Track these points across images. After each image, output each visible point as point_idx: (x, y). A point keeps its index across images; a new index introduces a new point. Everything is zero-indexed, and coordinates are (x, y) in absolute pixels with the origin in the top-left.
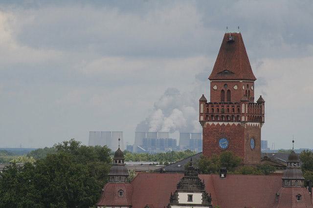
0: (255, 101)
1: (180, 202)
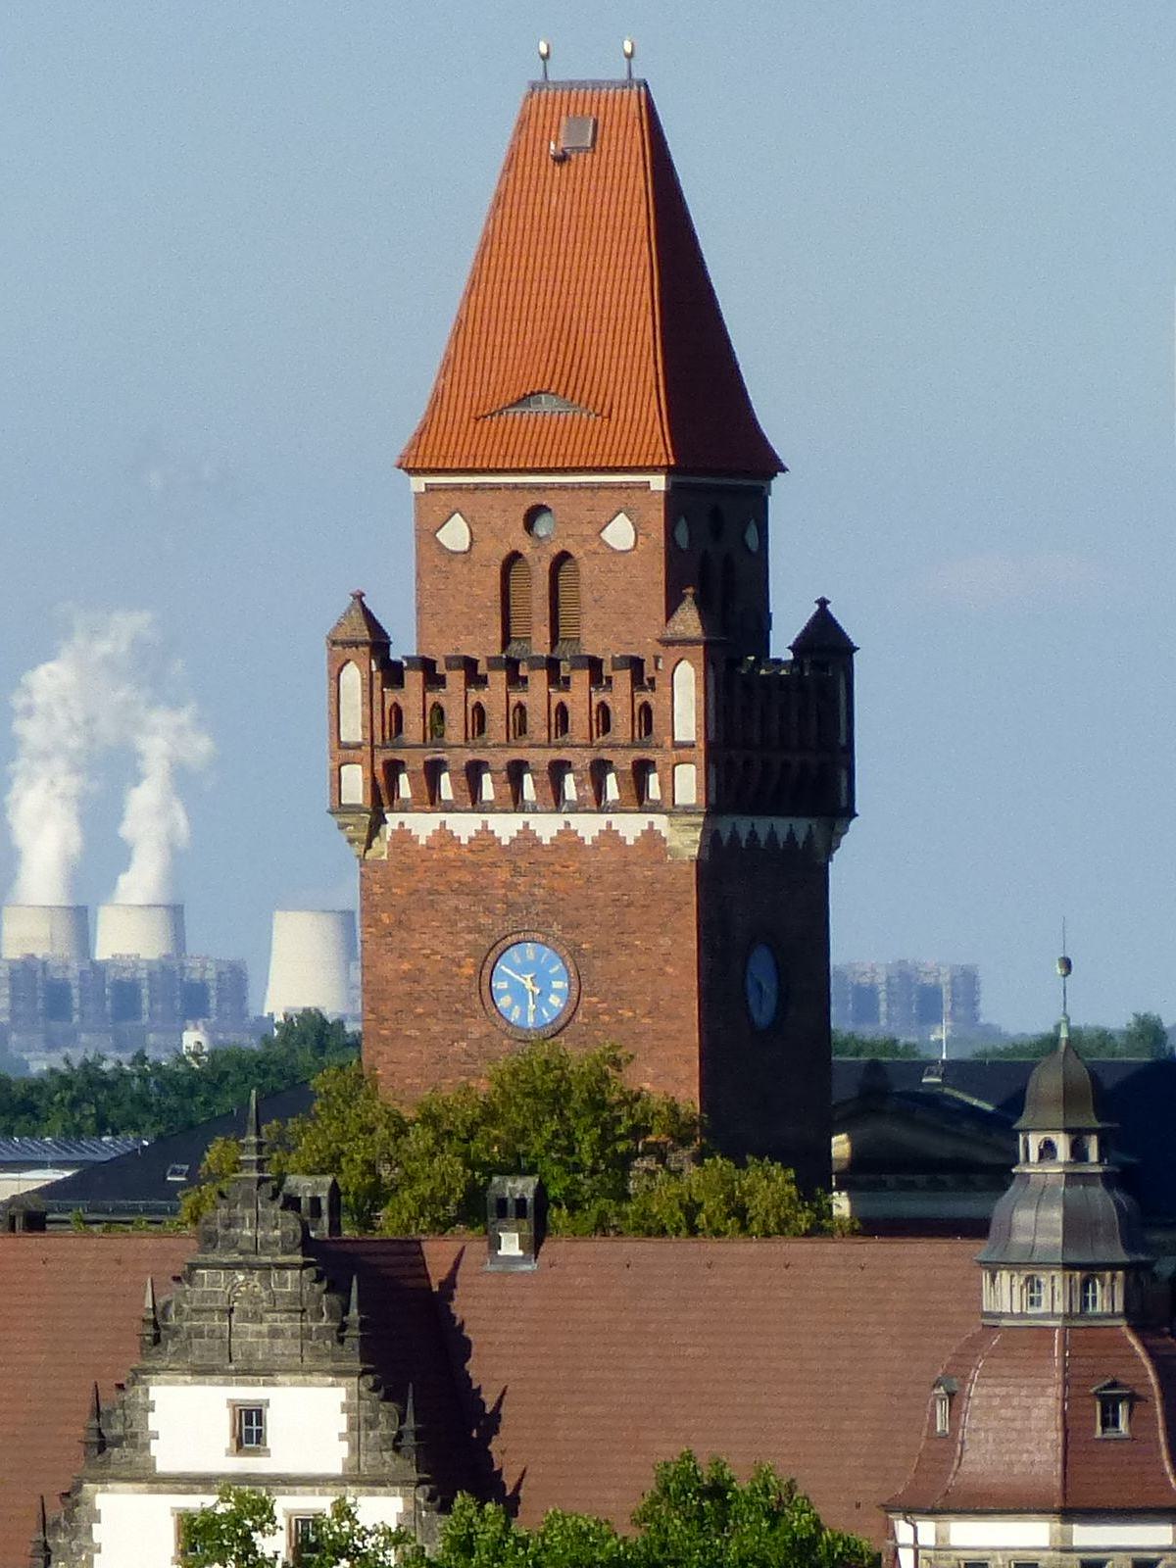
0: (781, 645)
1: (166, 1457)
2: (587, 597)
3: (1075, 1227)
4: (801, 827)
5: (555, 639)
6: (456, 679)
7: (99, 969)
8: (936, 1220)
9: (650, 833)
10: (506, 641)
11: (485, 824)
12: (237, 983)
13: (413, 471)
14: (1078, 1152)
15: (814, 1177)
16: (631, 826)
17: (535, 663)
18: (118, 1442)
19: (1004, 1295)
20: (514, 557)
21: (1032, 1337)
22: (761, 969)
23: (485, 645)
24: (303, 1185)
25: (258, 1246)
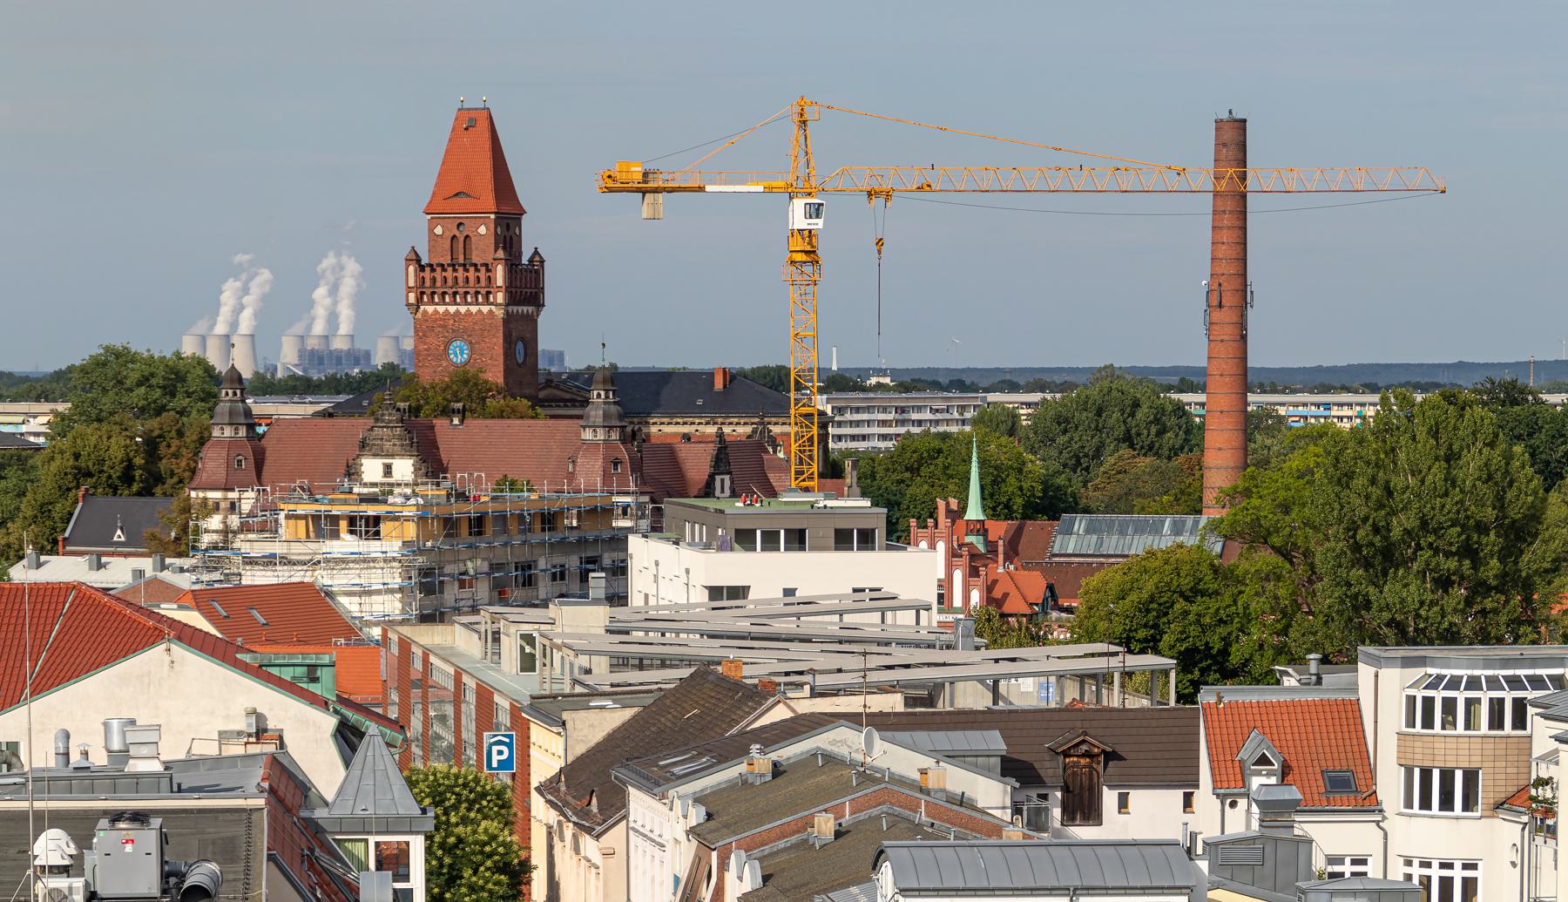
0: (525, 261)
1: (367, 478)
2: (473, 247)
3: (606, 416)
4: (530, 309)
5: (465, 259)
6: (439, 269)
7: (331, 352)
9: (491, 311)
10: (452, 259)
12: (367, 355)
13: (428, 214)
14: (607, 397)
17: (460, 265)
18: (353, 474)
19: (588, 435)
20: (454, 236)
21: (593, 445)
23: (446, 260)
24: (401, 405)
25: (390, 421)
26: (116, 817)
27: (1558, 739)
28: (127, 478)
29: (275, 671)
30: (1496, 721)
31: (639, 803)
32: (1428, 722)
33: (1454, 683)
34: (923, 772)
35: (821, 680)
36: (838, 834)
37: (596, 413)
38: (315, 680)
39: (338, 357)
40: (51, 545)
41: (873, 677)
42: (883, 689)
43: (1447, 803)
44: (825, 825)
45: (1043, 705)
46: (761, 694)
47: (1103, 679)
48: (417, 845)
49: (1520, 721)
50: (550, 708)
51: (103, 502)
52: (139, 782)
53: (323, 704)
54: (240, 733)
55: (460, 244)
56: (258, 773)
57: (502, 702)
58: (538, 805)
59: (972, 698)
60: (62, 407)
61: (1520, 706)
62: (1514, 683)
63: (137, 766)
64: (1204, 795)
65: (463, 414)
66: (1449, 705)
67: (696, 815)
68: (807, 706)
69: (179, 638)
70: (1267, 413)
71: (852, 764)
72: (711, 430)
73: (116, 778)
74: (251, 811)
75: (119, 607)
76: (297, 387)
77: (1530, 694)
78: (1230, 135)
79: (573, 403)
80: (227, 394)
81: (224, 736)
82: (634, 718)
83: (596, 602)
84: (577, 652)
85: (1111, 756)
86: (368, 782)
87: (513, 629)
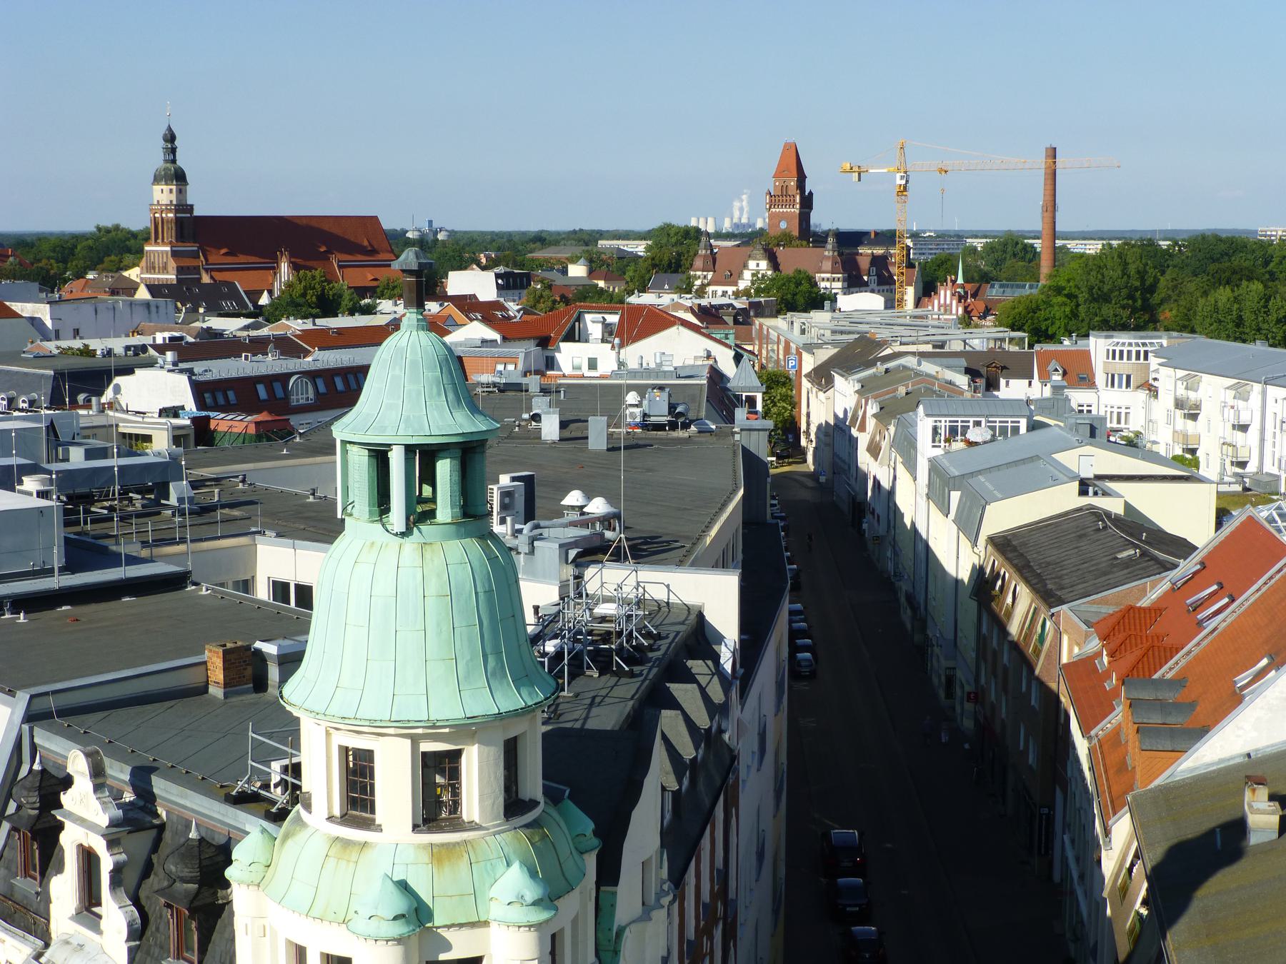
1: (750, 268)
8: (1238, 330)
11: (806, 376)
12: (754, 225)
15: (809, 242)
16: (793, 210)
19: (826, 253)
21: (828, 258)
22: (804, 226)
26: (654, 387)
27: (1160, 365)
28: (670, 265)
29: (714, 335)
30: (1138, 358)
31: (838, 379)
32: (1114, 358)
33: (1123, 344)
34: (937, 372)
35: (904, 340)
36: (907, 394)
37: (829, 246)
38: (727, 339)
39: (744, 226)
40: (643, 289)
41: (920, 339)
42: (927, 343)
43: (1120, 386)
44: (902, 391)
45: (981, 349)
46: (882, 344)
47: (1002, 340)
48: (759, 397)
49: (1146, 358)
50: (810, 348)
51: (662, 275)
52: (665, 374)
53: (730, 347)
54: (701, 357)
55: (784, 189)
56: (705, 373)
57: (793, 346)
58: (804, 381)
59: (957, 346)
60: (650, 242)
61: (1146, 353)
62: (1144, 344)
63: (666, 369)
64: (1036, 381)
65: (784, 246)
66: (1121, 352)
67: (858, 386)
68: (897, 348)
69: (682, 325)
70: (1064, 247)
71: (913, 370)
72: (870, 251)
73: (658, 373)
74: (702, 385)
75: (660, 313)
76: (729, 236)
77: (1149, 348)
78: (1050, 153)
79: (25, 873)
80: (703, 239)
81: (696, 358)
82: (551, 730)
83: (827, 311)
84: (820, 329)
85: (1004, 368)
86: (743, 375)
87: (798, 320)
